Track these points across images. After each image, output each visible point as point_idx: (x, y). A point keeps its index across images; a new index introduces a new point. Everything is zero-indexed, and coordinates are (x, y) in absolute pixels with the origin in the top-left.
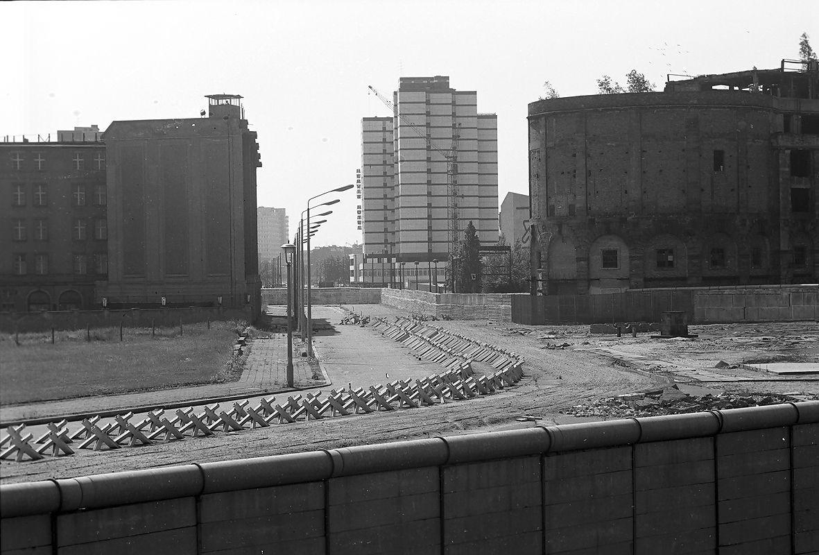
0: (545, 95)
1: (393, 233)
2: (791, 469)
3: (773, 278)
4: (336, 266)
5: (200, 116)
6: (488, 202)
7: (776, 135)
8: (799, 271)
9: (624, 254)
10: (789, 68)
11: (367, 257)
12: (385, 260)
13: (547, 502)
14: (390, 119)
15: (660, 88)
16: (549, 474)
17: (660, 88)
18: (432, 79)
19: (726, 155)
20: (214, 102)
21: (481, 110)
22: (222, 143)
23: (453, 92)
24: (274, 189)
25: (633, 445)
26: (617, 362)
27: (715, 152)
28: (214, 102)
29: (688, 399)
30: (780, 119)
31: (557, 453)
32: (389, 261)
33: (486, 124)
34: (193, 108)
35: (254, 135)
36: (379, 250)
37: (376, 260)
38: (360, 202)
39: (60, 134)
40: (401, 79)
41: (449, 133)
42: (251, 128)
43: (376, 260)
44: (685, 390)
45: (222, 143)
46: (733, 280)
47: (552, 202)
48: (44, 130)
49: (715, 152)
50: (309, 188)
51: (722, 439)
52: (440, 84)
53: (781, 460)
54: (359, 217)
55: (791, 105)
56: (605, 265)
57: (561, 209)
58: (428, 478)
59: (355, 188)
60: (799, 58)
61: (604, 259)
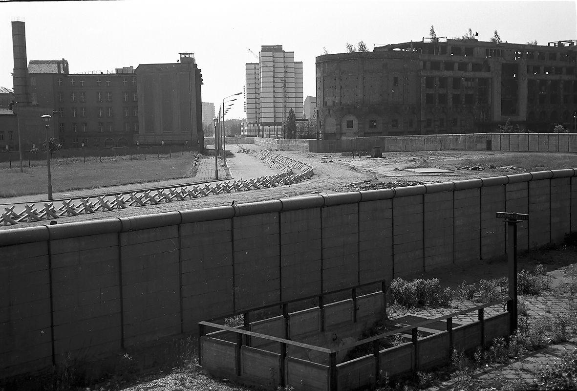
2: (423, 212)
6: (298, 100)
9: (356, 122)
10: (426, 41)
16: (324, 215)
17: (371, 50)
19: (399, 79)
20: (182, 56)
21: (296, 60)
22: (187, 73)
23: (284, 52)
24: (208, 95)
25: (358, 203)
26: (353, 168)
28: (182, 56)
29: (382, 184)
30: (422, 63)
32: (258, 125)
34: (174, 58)
35: (200, 70)
36: (253, 121)
38: (245, 100)
39: (117, 70)
40: (262, 46)
41: (282, 70)
42: (199, 67)
44: (381, 180)
45: (187, 73)
48: (109, 68)
50: (224, 94)
52: (278, 49)
53: (419, 208)
55: (426, 57)
56: (348, 127)
57: (330, 103)
59: (243, 94)
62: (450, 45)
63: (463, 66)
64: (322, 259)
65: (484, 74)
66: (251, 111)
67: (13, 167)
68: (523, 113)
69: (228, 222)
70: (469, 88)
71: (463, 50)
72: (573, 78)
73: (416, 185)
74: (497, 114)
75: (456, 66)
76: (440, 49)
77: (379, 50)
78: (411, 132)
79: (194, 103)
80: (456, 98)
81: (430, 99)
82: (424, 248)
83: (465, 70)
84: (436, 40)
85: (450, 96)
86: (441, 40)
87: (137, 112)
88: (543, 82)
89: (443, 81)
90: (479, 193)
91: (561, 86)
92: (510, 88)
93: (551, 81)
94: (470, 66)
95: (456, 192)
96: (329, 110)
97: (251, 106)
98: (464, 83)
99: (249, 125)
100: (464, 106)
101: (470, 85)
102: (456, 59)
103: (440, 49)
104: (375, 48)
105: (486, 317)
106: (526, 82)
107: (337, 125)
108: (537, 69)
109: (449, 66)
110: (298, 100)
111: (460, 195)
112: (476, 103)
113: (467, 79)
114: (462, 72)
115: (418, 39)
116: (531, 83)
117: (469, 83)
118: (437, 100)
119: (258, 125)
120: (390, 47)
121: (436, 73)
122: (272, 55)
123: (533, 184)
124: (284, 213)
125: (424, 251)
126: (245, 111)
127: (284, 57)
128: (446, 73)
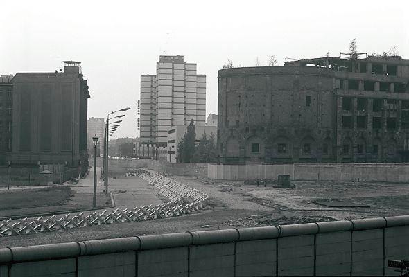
0: (227, 64)
1: (155, 132)
2: (315, 256)
3: (333, 159)
4: (126, 147)
7: (336, 89)
8: (345, 157)
10: (343, 57)
13: (190, 270)
14: (155, 76)
15: (282, 65)
16: (192, 257)
17: (282, 65)
19: (312, 98)
20: (67, 65)
21: (198, 73)
22: (71, 85)
23: (185, 64)
24: (95, 109)
26: (254, 199)
27: (307, 97)
28: (67, 65)
29: (285, 219)
30: (338, 82)
31: (197, 245)
32: (152, 146)
33: (201, 79)
34: (56, 66)
36: (146, 140)
37: (146, 145)
38: (139, 116)
41: (183, 83)
43: (146, 145)
44: (286, 214)
45: (71, 85)
46: (314, 160)
47: (228, 119)
49: (307, 97)
50: (114, 107)
51: (280, 240)
52: (179, 60)
53: (310, 251)
55: (344, 75)
57: (233, 123)
60: (350, 52)
61: (253, 148)
62: (371, 62)
63: (384, 87)
67: (115, 175)
69: (72, 262)
70: (392, 110)
71: (385, 68)
72: (406, 96)
73: (323, 221)
75: (377, 85)
76: (359, 65)
77: (290, 65)
78: (325, 159)
80: (377, 123)
81: (347, 122)
83: (357, 88)
84: (355, 55)
85: (370, 120)
86: (361, 57)
87: (11, 127)
89: (362, 102)
90: (382, 234)
93: (358, 98)
94: (392, 87)
95: (354, 233)
97: (145, 123)
99: (143, 145)
101: (391, 108)
102: (378, 78)
103: (359, 65)
104: (286, 63)
107: (240, 148)
109: (369, 86)
111: (358, 236)
113: (390, 101)
114: (384, 93)
115: (334, 55)
118: (355, 124)
119: (148, 146)
120: (303, 63)
121: (354, 93)
123: (320, 239)
124: (142, 252)
127: (185, 69)
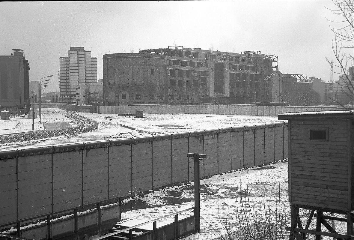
5: (11, 55)
6: (94, 81)
9: (128, 96)
10: (170, 48)
11: (62, 95)
12: (66, 96)
14: (68, 58)
18: (79, 47)
19: (154, 70)
20: (15, 51)
21: (92, 56)
23: (85, 51)
25: (53, 153)
27: (152, 69)
30: (168, 62)
32: (68, 96)
34: (9, 53)
40: (70, 47)
49: (152, 69)
52: (81, 49)
54: (59, 84)
56: (123, 98)
57: (111, 84)
58: (282, 128)
61: (123, 97)
63: (192, 64)
64: (83, 184)
65: (205, 69)
66: (63, 87)
68: (227, 94)
73: (160, 134)
74: (212, 94)
79: (22, 82)
80: (188, 83)
81: (173, 83)
82: (152, 175)
85: (185, 81)
88: (238, 75)
91: (249, 77)
92: (219, 77)
96: (111, 88)
98: (193, 74)
100: (193, 87)
101: (196, 75)
104: (140, 51)
105: (179, 219)
106: (228, 74)
108: (234, 67)
109: (184, 64)
110: (94, 81)
112: (200, 86)
113: (195, 72)
115: (165, 47)
116: (231, 75)
117: (196, 74)
118: (177, 83)
119: (68, 96)
120: (149, 51)
122: (77, 53)
125: (152, 177)
126: (59, 87)
128: (183, 68)
